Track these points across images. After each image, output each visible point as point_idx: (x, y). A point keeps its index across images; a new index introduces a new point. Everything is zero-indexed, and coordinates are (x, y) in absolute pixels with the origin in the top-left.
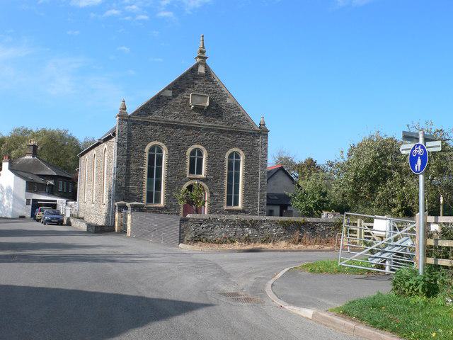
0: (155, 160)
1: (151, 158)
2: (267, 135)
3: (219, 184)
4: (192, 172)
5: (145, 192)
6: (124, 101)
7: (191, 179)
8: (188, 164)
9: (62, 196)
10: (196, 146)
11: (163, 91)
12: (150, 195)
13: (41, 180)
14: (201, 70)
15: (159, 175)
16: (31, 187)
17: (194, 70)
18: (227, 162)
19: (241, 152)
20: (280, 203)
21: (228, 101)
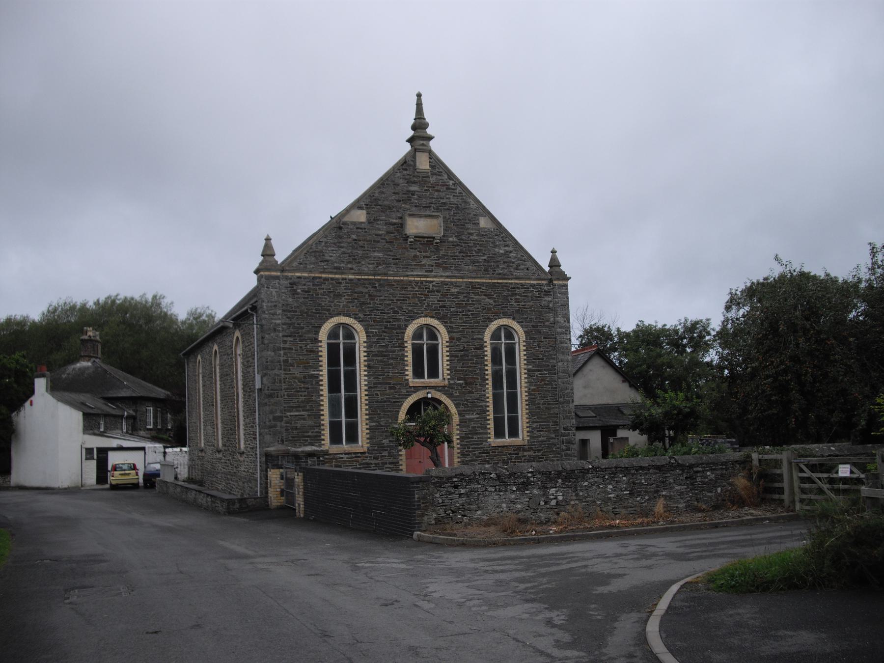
0: (341, 355)
1: (333, 350)
2: (566, 286)
3: (476, 395)
4: (418, 373)
5: (491, 417)
6: (554, 252)
7: (417, 389)
8: (409, 358)
9: (155, 439)
10: (423, 321)
11: (347, 211)
12: (335, 427)
13: (110, 409)
14: (423, 163)
15: (351, 385)
16: (91, 423)
17: (406, 165)
18: (488, 349)
19: (358, 327)
20: (601, 424)
21: (483, 223)
